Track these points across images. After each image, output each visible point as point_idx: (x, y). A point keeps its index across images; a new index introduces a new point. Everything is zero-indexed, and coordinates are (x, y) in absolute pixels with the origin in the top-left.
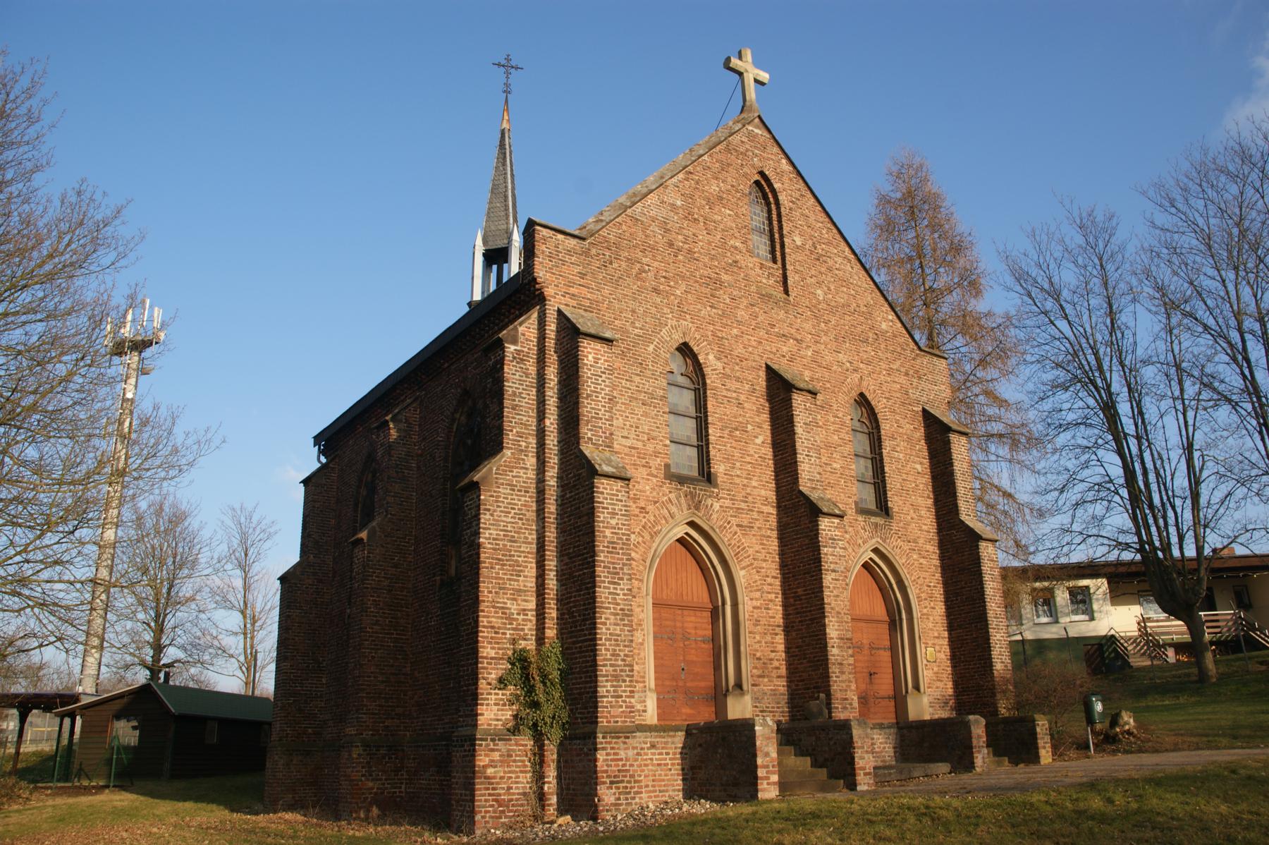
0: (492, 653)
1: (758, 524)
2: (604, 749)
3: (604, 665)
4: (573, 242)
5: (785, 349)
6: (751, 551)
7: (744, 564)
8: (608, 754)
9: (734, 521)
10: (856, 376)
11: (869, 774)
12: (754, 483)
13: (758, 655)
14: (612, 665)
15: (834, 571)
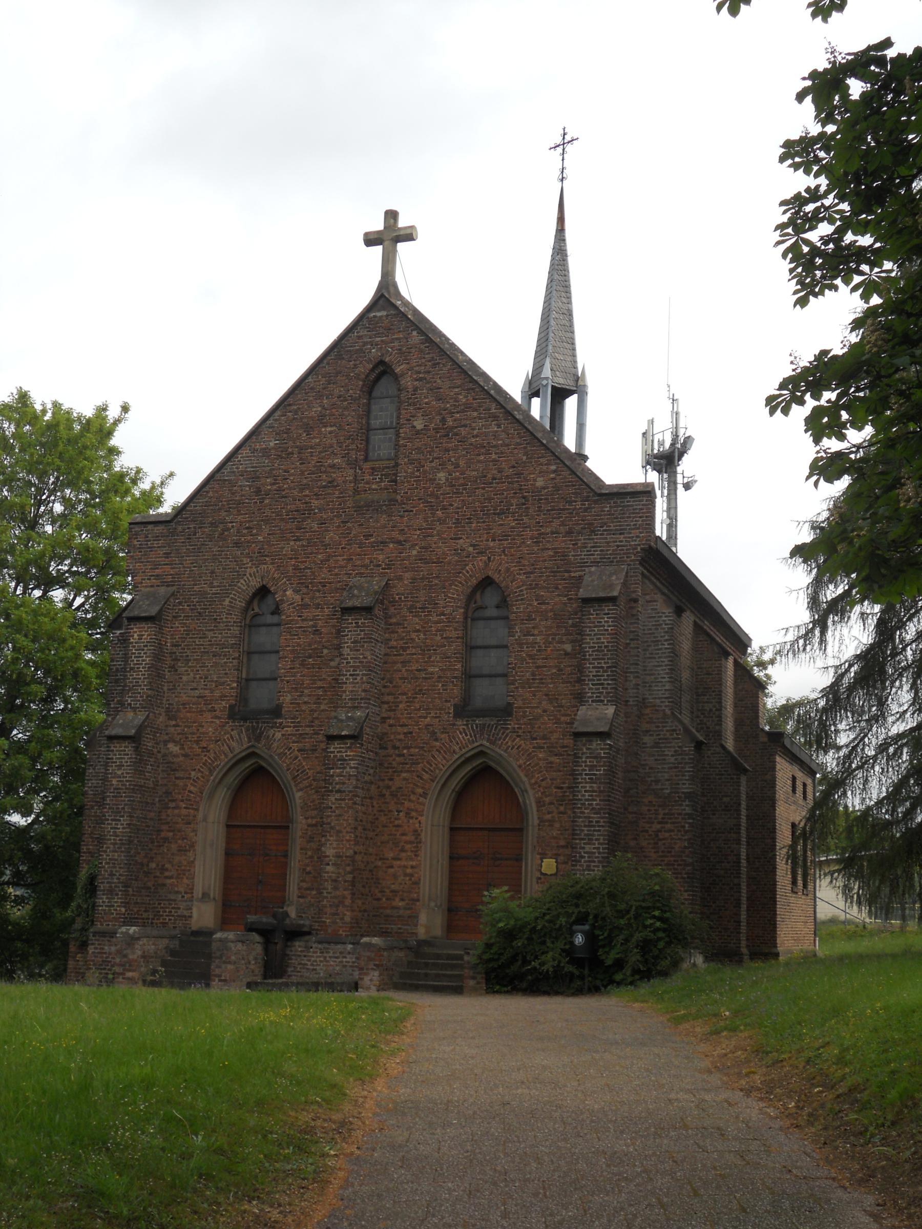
2: (93, 944)
3: (102, 883)
4: (161, 528)
8: (96, 948)
9: (295, 746)
11: (216, 976)
13: (308, 869)
14: (108, 883)
15: (339, 791)
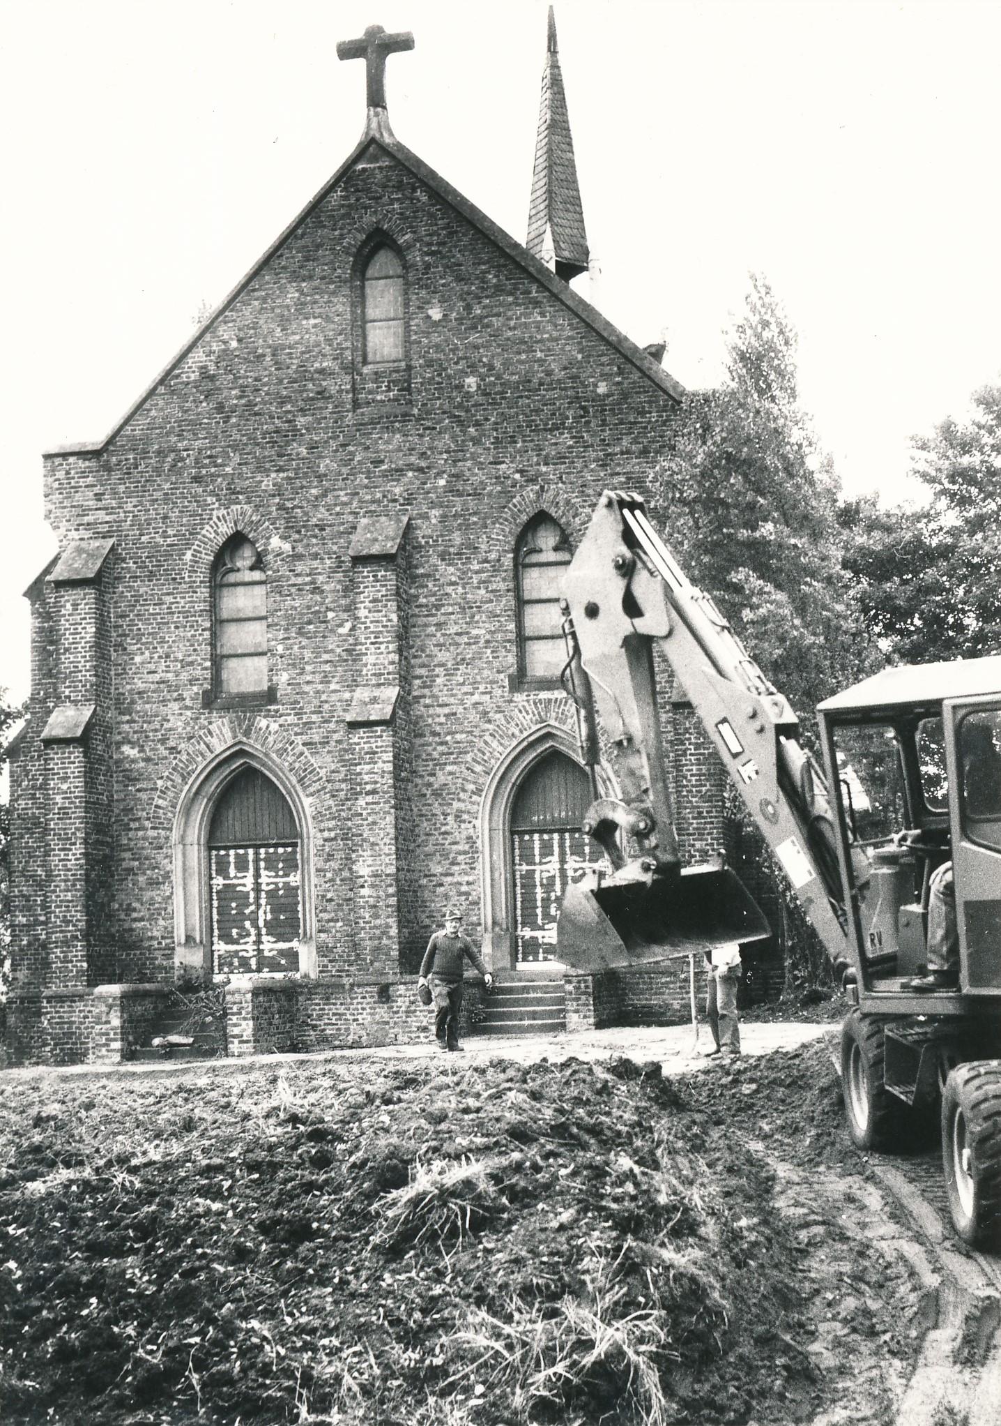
0: (24, 920)
1: (336, 737)
5: (397, 490)
6: (322, 773)
7: (311, 789)
9: (299, 740)
10: (531, 492)
12: (333, 687)
13: (329, 895)
